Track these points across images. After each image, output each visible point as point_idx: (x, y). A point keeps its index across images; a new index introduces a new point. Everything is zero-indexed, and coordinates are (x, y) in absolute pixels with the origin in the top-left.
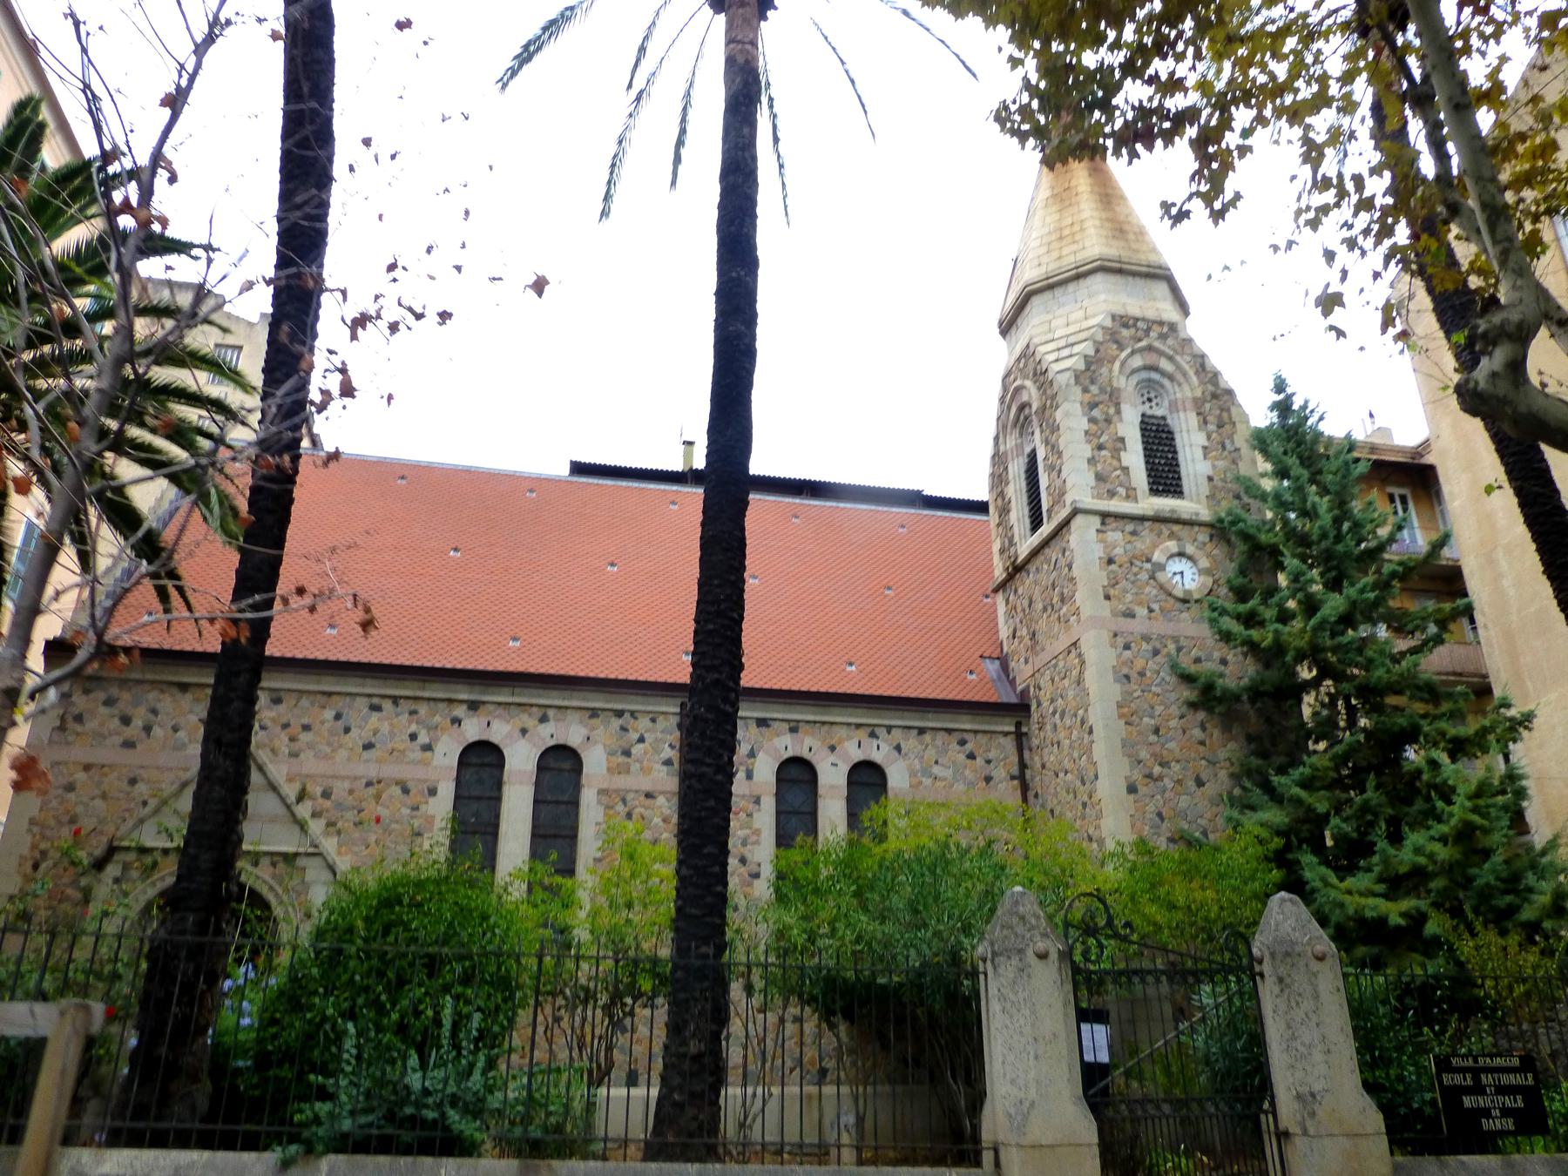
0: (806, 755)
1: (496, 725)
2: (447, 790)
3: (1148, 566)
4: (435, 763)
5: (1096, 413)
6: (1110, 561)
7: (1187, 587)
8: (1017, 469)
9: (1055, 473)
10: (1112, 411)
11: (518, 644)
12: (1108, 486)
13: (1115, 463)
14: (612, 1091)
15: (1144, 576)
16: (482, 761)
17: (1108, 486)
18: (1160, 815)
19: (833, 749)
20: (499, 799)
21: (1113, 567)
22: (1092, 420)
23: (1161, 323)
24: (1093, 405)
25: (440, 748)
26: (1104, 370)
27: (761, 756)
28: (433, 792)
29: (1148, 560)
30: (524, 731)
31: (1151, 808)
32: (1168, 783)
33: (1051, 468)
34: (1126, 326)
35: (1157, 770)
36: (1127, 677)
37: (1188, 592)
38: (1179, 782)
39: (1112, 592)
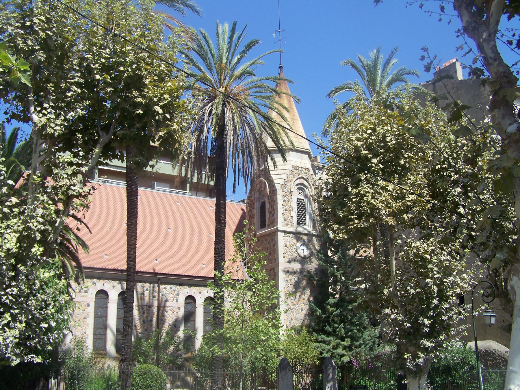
0: (193, 295)
1: (106, 284)
2: (92, 305)
3: (295, 247)
4: (89, 297)
5: (286, 199)
6: (286, 246)
7: (305, 254)
8: (257, 205)
9: (271, 215)
10: (290, 198)
11: (107, 256)
12: (287, 222)
13: (289, 215)
14: (479, 342)
15: (294, 250)
16: (102, 294)
17: (287, 222)
18: (292, 319)
19: (200, 293)
20: (107, 307)
21: (286, 248)
22: (285, 201)
23: (305, 169)
24: (285, 196)
25: (90, 292)
26: (289, 184)
27: (180, 295)
28: (89, 305)
29: (295, 246)
30: (114, 287)
31: (290, 317)
32: (294, 310)
33: (270, 212)
34: (296, 169)
35: (292, 307)
36: (287, 280)
37: (305, 256)
38: (297, 310)
39: (285, 255)
